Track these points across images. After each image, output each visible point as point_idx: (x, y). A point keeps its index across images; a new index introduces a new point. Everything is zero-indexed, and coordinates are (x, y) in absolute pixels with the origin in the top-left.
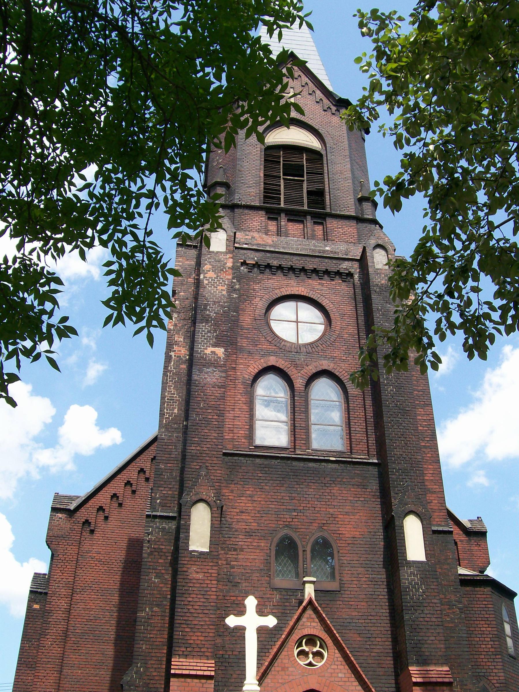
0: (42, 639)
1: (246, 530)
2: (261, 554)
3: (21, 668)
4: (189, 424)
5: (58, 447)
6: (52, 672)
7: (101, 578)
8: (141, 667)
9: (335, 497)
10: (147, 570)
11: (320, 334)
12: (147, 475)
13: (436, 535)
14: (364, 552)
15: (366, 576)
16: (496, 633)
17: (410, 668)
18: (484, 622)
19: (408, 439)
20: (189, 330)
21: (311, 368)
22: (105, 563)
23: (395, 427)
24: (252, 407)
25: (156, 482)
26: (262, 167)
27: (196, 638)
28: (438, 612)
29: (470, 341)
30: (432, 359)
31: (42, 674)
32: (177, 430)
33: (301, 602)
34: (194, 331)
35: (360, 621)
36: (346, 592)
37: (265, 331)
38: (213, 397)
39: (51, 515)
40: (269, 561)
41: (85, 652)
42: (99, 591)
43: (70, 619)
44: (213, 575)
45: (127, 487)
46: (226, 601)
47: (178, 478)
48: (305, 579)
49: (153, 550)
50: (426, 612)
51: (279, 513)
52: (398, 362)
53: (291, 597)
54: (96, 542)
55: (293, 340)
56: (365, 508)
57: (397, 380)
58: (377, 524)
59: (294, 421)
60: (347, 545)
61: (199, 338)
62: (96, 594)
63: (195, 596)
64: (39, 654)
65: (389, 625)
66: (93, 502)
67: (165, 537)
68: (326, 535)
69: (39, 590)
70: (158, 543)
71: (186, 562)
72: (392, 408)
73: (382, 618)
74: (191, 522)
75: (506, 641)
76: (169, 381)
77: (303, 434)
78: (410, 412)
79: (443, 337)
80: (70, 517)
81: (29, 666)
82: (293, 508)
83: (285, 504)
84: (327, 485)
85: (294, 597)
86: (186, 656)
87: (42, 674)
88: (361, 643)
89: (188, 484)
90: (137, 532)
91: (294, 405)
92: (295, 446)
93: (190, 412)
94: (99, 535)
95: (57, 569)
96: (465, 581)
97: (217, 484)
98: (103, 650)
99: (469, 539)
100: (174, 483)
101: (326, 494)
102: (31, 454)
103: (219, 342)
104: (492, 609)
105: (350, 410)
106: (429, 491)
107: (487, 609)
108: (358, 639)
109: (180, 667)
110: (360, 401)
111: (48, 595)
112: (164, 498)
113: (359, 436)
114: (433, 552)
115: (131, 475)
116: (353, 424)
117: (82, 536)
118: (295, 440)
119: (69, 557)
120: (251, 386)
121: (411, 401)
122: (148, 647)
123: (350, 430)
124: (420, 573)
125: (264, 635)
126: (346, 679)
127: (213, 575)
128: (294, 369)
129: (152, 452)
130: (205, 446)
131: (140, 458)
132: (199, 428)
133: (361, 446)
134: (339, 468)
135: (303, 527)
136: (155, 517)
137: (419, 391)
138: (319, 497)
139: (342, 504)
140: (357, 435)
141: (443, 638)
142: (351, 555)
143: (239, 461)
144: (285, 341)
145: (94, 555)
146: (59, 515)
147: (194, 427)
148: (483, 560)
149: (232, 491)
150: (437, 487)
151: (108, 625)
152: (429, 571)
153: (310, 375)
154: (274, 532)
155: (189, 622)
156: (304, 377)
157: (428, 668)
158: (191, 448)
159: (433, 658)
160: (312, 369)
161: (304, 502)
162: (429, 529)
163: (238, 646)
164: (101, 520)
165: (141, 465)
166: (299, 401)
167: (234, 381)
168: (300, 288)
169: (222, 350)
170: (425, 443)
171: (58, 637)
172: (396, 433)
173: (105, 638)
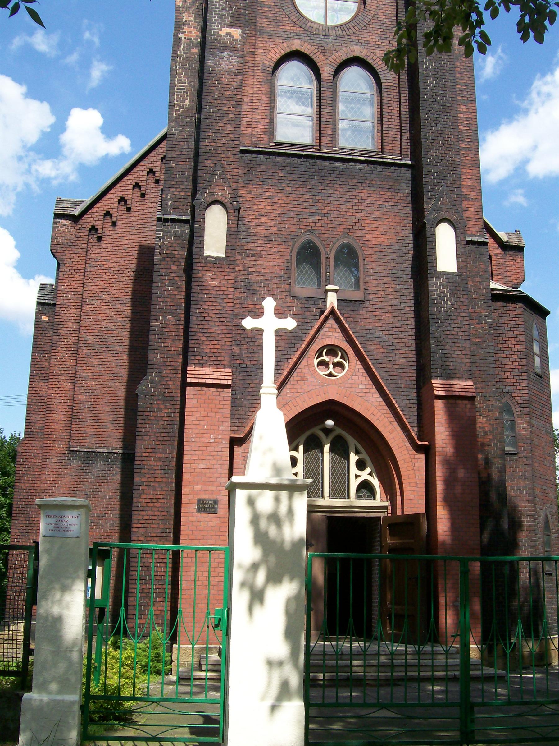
0: (53, 351)
1: (265, 235)
2: (281, 261)
3: (34, 380)
4: (202, 116)
5: (60, 157)
6: (66, 384)
7: (111, 288)
8: (156, 376)
10: (160, 277)
11: (353, 14)
12: (157, 176)
13: (470, 246)
14: (392, 261)
15: (393, 286)
16: (524, 350)
17: (433, 381)
18: (512, 339)
19: (447, 139)
20: (201, 7)
21: (340, 54)
22: (115, 272)
23: (433, 125)
24: (272, 98)
25: (166, 182)
27: (212, 347)
28: (466, 326)
29: (527, 20)
30: (480, 40)
31: (56, 386)
32: (189, 124)
33: (322, 312)
34: (206, 8)
35: (384, 332)
36: (371, 302)
37: (288, 9)
38: (229, 86)
39: (54, 222)
40: (289, 268)
41: (98, 363)
42: (110, 301)
43: (81, 331)
44: (230, 281)
45: (135, 190)
46: (243, 310)
47: (191, 178)
48: (327, 287)
49: (165, 255)
50: (453, 325)
51: (300, 217)
52: (440, 42)
53: (312, 306)
54: (104, 250)
55: (321, 21)
56: (395, 214)
57: (438, 70)
58: (408, 232)
59: (320, 115)
60: (373, 253)
61: (212, 17)
62: (107, 304)
63: (210, 303)
64: (51, 365)
65: (414, 337)
66: (99, 206)
67: (178, 242)
68: (351, 241)
69: (47, 301)
70: (171, 248)
71: (200, 268)
72: (430, 103)
73: (407, 330)
74: (206, 226)
75: (534, 359)
76: (179, 68)
77: (329, 129)
78: (451, 108)
79: (494, 14)
80: (75, 224)
81: (41, 378)
82: (317, 211)
83: (308, 207)
84: (354, 187)
85: (316, 306)
86: (202, 365)
87: (56, 386)
88: (384, 354)
89: (202, 184)
90: (149, 239)
91: (320, 96)
92: (320, 143)
93: (203, 103)
94: (107, 242)
95: (64, 279)
96: (497, 297)
97: (234, 184)
98: (116, 361)
99: (505, 254)
100: (186, 183)
101: (353, 197)
102: (30, 165)
103: (236, 22)
104: (523, 326)
105: (383, 104)
106: (466, 198)
107: (517, 326)
108: (382, 350)
109: (196, 376)
110: (395, 94)
111: (57, 306)
112: (176, 199)
113: (392, 133)
114: (465, 264)
115: (139, 176)
116: (386, 120)
117: (89, 244)
118: (320, 137)
119: (77, 266)
120: (273, 74)
121: (452, 96)
122: (162, 356)
123: (382, 127)
124: (450, 284)
125: (283, 345)
126: (367, 391)
127: (230, 281)
128: (321, 55)
129: (162, 151)
130: (220, 142)
131: (149, 157)
132: (214, 121)
133: (394, 145)
134: (368, 168)
135: (327, 232)
136: (167, 220)
137: (462, 85)
138: (345, 200)
139: (369, 209)
140: (390, 132)
141: (469, 353)
142: (377, 264)
143: (257, 159)
144: (312, 22)
145: (103, 263)
146: (63, 221)
147: (208, 121)
148: (518, 276)
149: (250, 193)
150: (475, 194)
151: (121, 335)
152: (459, 283)
153: (340, 62)
154: (296, 237)
155: (205, 331)
156: (333, 64)
157: (452, 382)
158: (205, 144)
159: (457, 372)
160: (342, 56)
161: (329, 205)
162: (463, 239)
163: (257, 355)
164: (108, 226)
165: (150, 165)
166: (327, 93)
167: (252, 68)
169: (239, 31)
170: (465, 145)
171: (70, 349)
172: (433, 131)
173: (117, 350)
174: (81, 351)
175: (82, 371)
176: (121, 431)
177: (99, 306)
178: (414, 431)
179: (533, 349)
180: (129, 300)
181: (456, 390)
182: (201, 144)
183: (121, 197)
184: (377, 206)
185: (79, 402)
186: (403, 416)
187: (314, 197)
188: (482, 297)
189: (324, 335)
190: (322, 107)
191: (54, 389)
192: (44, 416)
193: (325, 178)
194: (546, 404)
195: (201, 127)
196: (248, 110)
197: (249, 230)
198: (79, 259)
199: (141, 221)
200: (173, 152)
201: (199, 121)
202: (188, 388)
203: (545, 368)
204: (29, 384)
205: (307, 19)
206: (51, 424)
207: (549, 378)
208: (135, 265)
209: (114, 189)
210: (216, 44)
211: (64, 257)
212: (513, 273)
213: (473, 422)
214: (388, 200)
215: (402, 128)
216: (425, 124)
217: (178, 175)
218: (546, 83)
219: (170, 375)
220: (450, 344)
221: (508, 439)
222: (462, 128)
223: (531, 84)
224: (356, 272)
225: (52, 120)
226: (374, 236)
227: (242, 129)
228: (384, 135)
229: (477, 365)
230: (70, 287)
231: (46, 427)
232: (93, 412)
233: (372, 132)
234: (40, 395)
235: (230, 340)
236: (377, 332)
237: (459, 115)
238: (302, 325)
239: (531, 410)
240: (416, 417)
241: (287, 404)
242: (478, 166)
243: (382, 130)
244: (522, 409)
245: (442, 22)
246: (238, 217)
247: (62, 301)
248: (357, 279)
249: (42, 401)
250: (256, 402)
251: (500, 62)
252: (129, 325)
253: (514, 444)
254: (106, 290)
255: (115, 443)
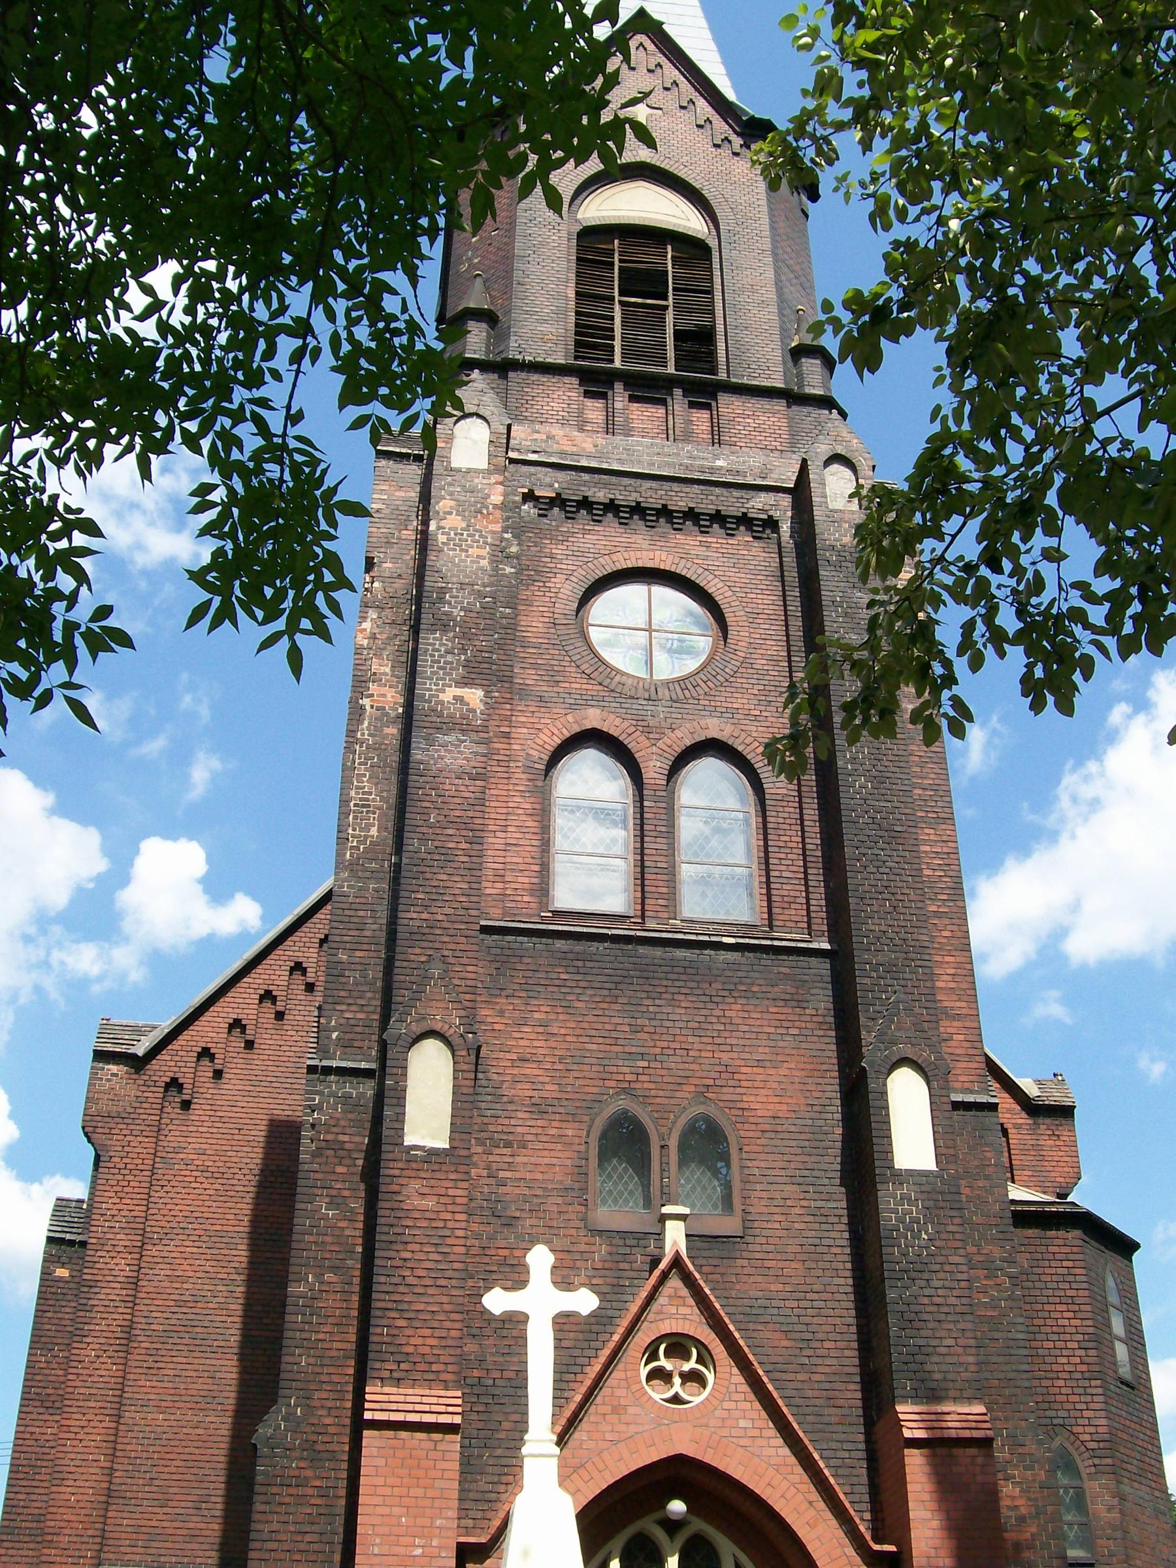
0: (75, 1345)
1: (533, 1100)
2: (567, 1154)
4: (405, 861)
6: (99, 1418)
7: (206, 1209)
8: (296, 1406)
9: (734, 1028)
10: (311, 1191)
12: (311, 977)
13: (961, 1112)
14: (799, 1151)
16: (1091, 1330)
17: (899, 1408)
18: (1064, 1307)
20: (405, 648)
21: (680, 735)
22: (216, 1175)
26: (573, 276)
27: (419, 1341)
28: (963, 1284)
29: (1039, 672)
30: (952, 713)
31: (78, 1423)
33: (655, 1262)
34: (415, 650)
36: (758, 1240)
39: (92, 1068)
40: (583, 1170)
41: (171, 1373)
42: (202, 1239)
44: (459, 1200)
45: (264, 1005)
47: (379, 984)
48: (665, 1210)
50: (935, 1283)
51: (606, 1062)
53: (634, 1250)
54: (195, 1129)
56: (802, 1052)
57: (875, 762)
58: (829, 1088)
59: (642, 854)
60: (759, 1134)
61: (426, 666)
62: (196, 1244)
63: (417, 1247)
64: (70, 1377)
66: (189, 1038)
67: (351, 1116)
68: (712, 1111)
69: (68, 1237)
70: (335, 1130)
71: (397, 1172)
73: (838, 1296)
74: (409, 1082)
75: (1113, 1349)
78: (906, 835)
79: (976, 664)
80: (137, 1072)
82: (639, 1050)
83: (620, 1042)
84: (714, 999)
85: (642, 1251)
86: (398, 1382)
87: (78, 1423)
88: (790, 1352)
89: (401, 996)
90: (290, 1106)
91: (642, 818)
92: (643, 910)
93: (406, 835)
94: (201, 1112)
95: (108, 1188)
97: (468, 997)
98: (212, 1369)
100: (369, 995)
101: (714, 1020)
104: (1084, 1278)
105: (769, 831)
106: (947, 1014)
107: (1071, 1278)
108: (785, 1343)
109: (384, 1406)
110: (792, 810)
111: (89, 1246)
112: (347, 1028)
113: (789, 887)
114: (952, 1151)
115: (273, 977)
117: (165, 1115)
118: (643, 898)
120: (546, 775)
121: (907, 811)
122: (312, 1361)
123: (768, 876)
124: (925, 1196)
126: (757, 1433)
132: (428, 869)
134: (743, 960)
135: (661, 1093)
136: (327, 1071)
139: (748, 1042)
140: (784, 886)
141: (972, 1342)
142: (770, 1157)
144: (623, 674)
146: (111, 1067)
147: (415, 869)
149: (501, 1013)
150: (964, 1004)
151: (224, 1312)
154: (597, 1105)
155: (405, 1306)
156: (666, 755)
158: (409, 915)
159: (951, 1385)
160: (684, 737)
161: (664, 1037)
162: (944, 1099)
163: (516, 1359)
168: (658, 553)
169: (480, 693)
170: (939, 906)
171: (112, 1341)
172: (872, 883)
173: (215, 1343)
174: (136, 1345)
175: (135, 1389)
176: (216, 1527)
177: (179, 1249)
178: (862, 1519)
179: (1109, 1326)
180: (245, 1235)
181: (950, 1424)
182: (401, 915)
183: (235, 1020)
184: (765, 1036)
185: (126, 1461)
186: (837, 1488)
187: (633, 1022)
188: (993, 1221)
189: (660, 1312)
190: (646, 839)
191: (72, 1429)
192: (46, 1491)
193: (656, 982)
194: (1150, 1447)
195: (403, 881)
196: (497, 847)
197: (499, 1092)
198: (141, 1146)
199: (275, 1069)
200: (344, 932)
201: (397, 868)
202: (366, 1433)
203: (1141, 1367)
204: (19, 1419)
205: (613, 669)
206: (61, 1510)
207: (1151, 1389)
208: (259, 1161)
209: (222, 1003)
210: (434, 719)
211: (109, 1142)
212: (1055, 1164)
213: (993, 1495)
214: (785, 1024)
215: (810, 877)
216: (854, 869)
217: (352, 977)
218: (1087, 779)
219: (330, 1404)
220: (930, 1325)
221: (1071, 1530)
222: (930, 872)
223: (1059, 782)
224: (724, 1171)
225: (101, 865)
226: (759, 1099)
227: (484, 884)
228: (774, 892)
229: (992, 1367)
230: (121, 1207)
231: (49, 1517)
232: (156, 1482)
233: (746, 821)
234: (41, 1443)
235: (458, 1325)
236: (774, 1303)
237: (923, 848)
238: (611, 1294)
239: (1118, 1463)
240: (865, 1489)
241: (582, 1466)
242: (966, 947)
243: (768, 883)
244: (1097, 1461)
245: (875, 681)
246: (477, 1064)
247: (101, 1235)
248: (728, 1186)
249: (45, 1457)
250: (514, 1462)
251: (996, 741)
252: (242, 1289)
253: (1087, 1542)
254: (195, 1214)
255: (201, 1553)
